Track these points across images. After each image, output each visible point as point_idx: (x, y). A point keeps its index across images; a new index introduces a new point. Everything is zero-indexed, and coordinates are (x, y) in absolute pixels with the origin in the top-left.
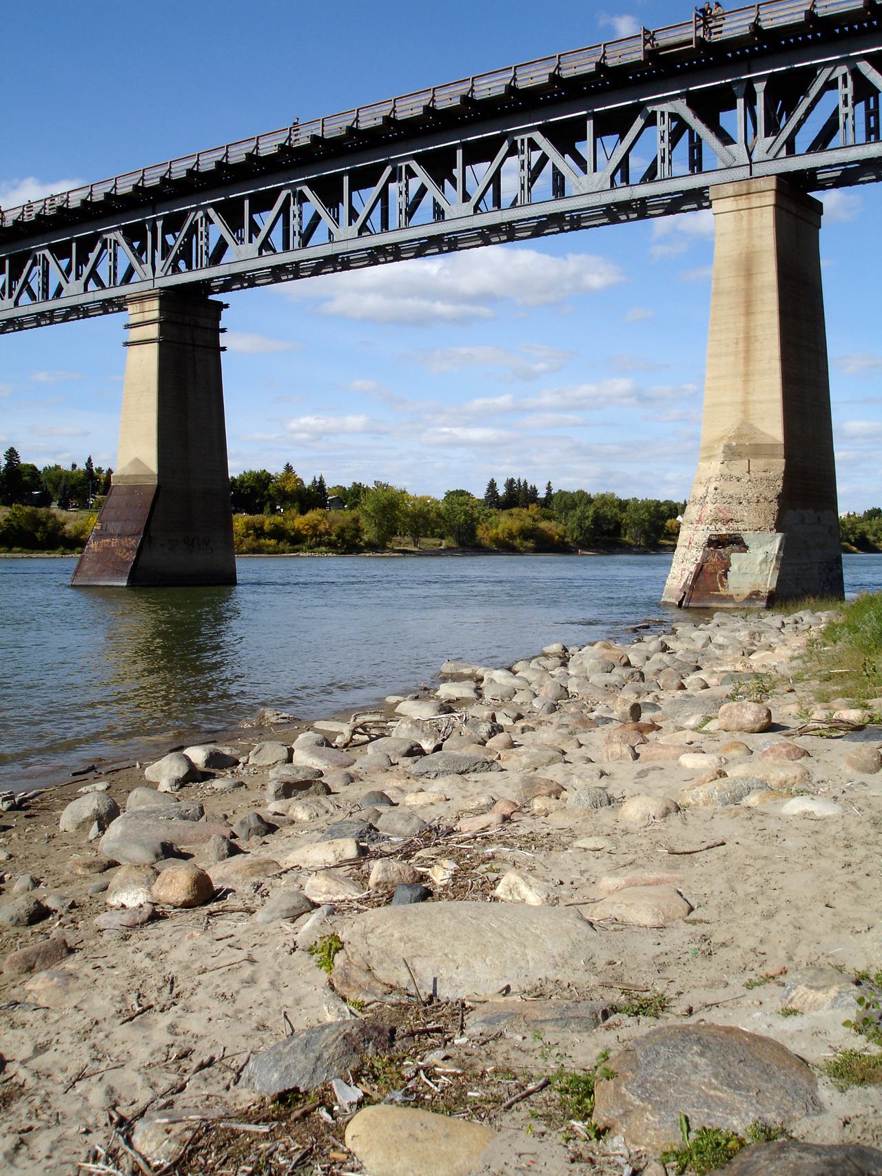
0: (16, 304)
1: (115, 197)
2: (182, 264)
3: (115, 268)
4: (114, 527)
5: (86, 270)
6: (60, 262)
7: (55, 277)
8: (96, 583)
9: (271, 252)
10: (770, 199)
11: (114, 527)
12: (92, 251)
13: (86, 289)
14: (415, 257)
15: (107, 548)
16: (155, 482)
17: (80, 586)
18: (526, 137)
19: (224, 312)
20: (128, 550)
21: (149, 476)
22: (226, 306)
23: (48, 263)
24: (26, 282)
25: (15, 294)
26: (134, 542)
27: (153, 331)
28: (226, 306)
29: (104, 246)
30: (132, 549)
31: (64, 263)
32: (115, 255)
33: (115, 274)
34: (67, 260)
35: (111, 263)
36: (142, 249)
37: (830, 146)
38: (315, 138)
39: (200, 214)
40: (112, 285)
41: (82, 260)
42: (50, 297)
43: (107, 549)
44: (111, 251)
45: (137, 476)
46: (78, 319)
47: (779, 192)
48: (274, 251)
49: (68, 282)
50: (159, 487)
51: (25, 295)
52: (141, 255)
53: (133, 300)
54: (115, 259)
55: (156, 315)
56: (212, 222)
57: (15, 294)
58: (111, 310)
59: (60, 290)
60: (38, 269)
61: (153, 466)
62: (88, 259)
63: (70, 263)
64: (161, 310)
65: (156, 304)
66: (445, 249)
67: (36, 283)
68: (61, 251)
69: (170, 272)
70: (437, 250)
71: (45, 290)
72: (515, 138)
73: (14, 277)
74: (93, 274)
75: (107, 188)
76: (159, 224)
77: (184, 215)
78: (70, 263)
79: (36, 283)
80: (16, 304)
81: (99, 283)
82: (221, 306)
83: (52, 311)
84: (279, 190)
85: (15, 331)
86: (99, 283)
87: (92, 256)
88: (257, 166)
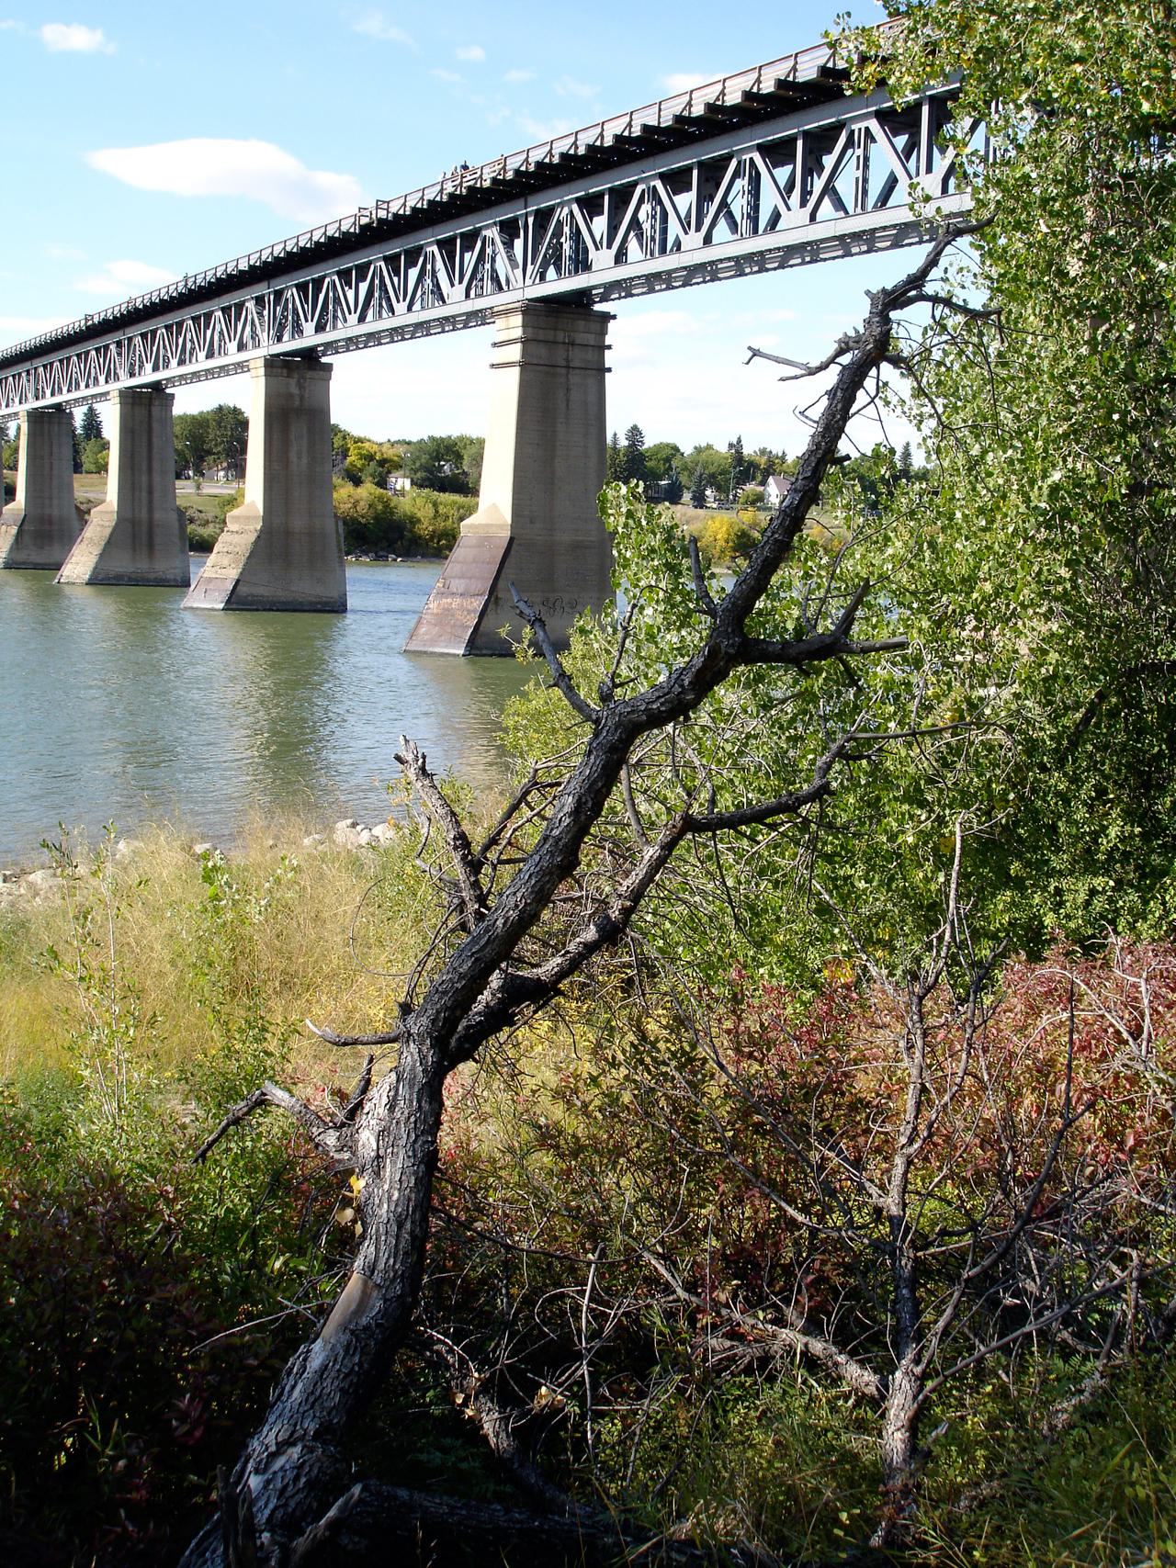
0: (813, 218)
1: (794, 86)
2: (551, 273)
3: (865, 180)
4: (458, 585)
5: (819, 184)
6: (774, 171)
7: (770, 198)
8: (431, 649)
9: (842, 214)
10: (262, 371)
11: (458, 585)
12: (830, 152)
13: (468, 296)
14: (683, 286)
15: (448, 610)
16: (507, 534)
17: (415, 652)
18: (862, 125)
19: (612, 325)
20: (469, 612)
21: (501, 526)
22: (614, 317)
23: (758, 174)
24: (724, 204)
25: (707, 221)
26: (478, 604)
27: (515, 352)
28: (614, 317)
29: (850, 143)
30: (474, 611)
31: (783, 173)
32: (866, 159)
33: (865, 192)
34: (789, 168)
35: (859, 174)
36: (912, 146)
37: (888, 205)
38: (646, 128)
39: (566, 210)
40: (859, 210)
41: (813, 167)
42: (760, 232)
43: (447, 611)
44: (860, 152)
45: (488, 525)
46: (704, 282)
47: (266, 366)
48: (846, 212)
49: (789, 209)
50: (512, 539)
51: (722, 224)
52: (908, 158)
53: (500, 313)
54: (866, 167)
55: (518, 333)
56: (874, 140)
57: (707, 221)
58: (854, 250)
59: (776, 217)
60: (742, 184)
61: (507, 517)
62: (822, 168)
63: (794, 171)
64: (524, 326)
65: (517, 320)
66: (808, 259)
67: (739, 205)
68: (778, 153)
69: (537, 281)
70: (799, 261)
71: (754, 218)
72: (853, 127)
73: (704, 197)
74: (829, 190)
75: (781, 71)
76: (531, 220)
77: (551, 210)
78: (794, 171)
79: (739, 205)
80: (813, 218)
81: (839, 204)
82: (607, 317)
83: (669, 273)
84: (635, 184)
85: (803, 263)
86: (839, 204)
87: (829, 161)
88: (719, 121)
